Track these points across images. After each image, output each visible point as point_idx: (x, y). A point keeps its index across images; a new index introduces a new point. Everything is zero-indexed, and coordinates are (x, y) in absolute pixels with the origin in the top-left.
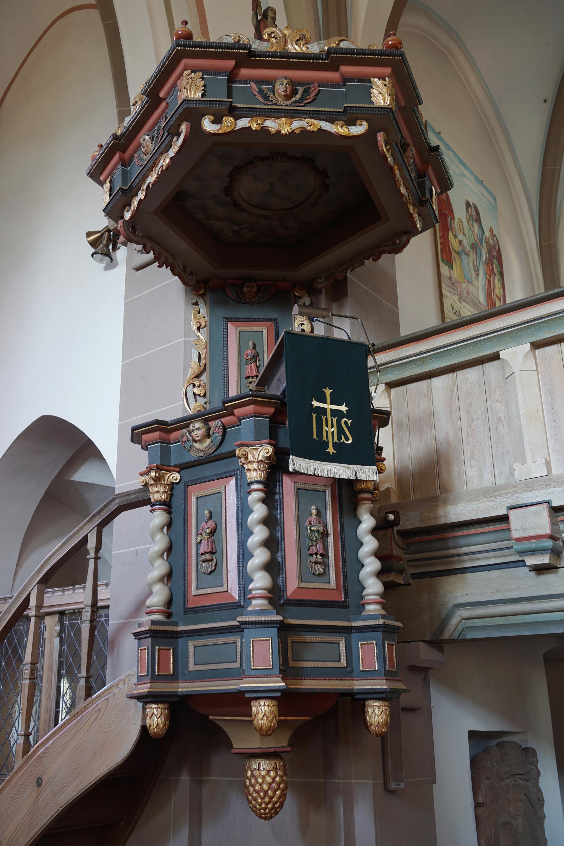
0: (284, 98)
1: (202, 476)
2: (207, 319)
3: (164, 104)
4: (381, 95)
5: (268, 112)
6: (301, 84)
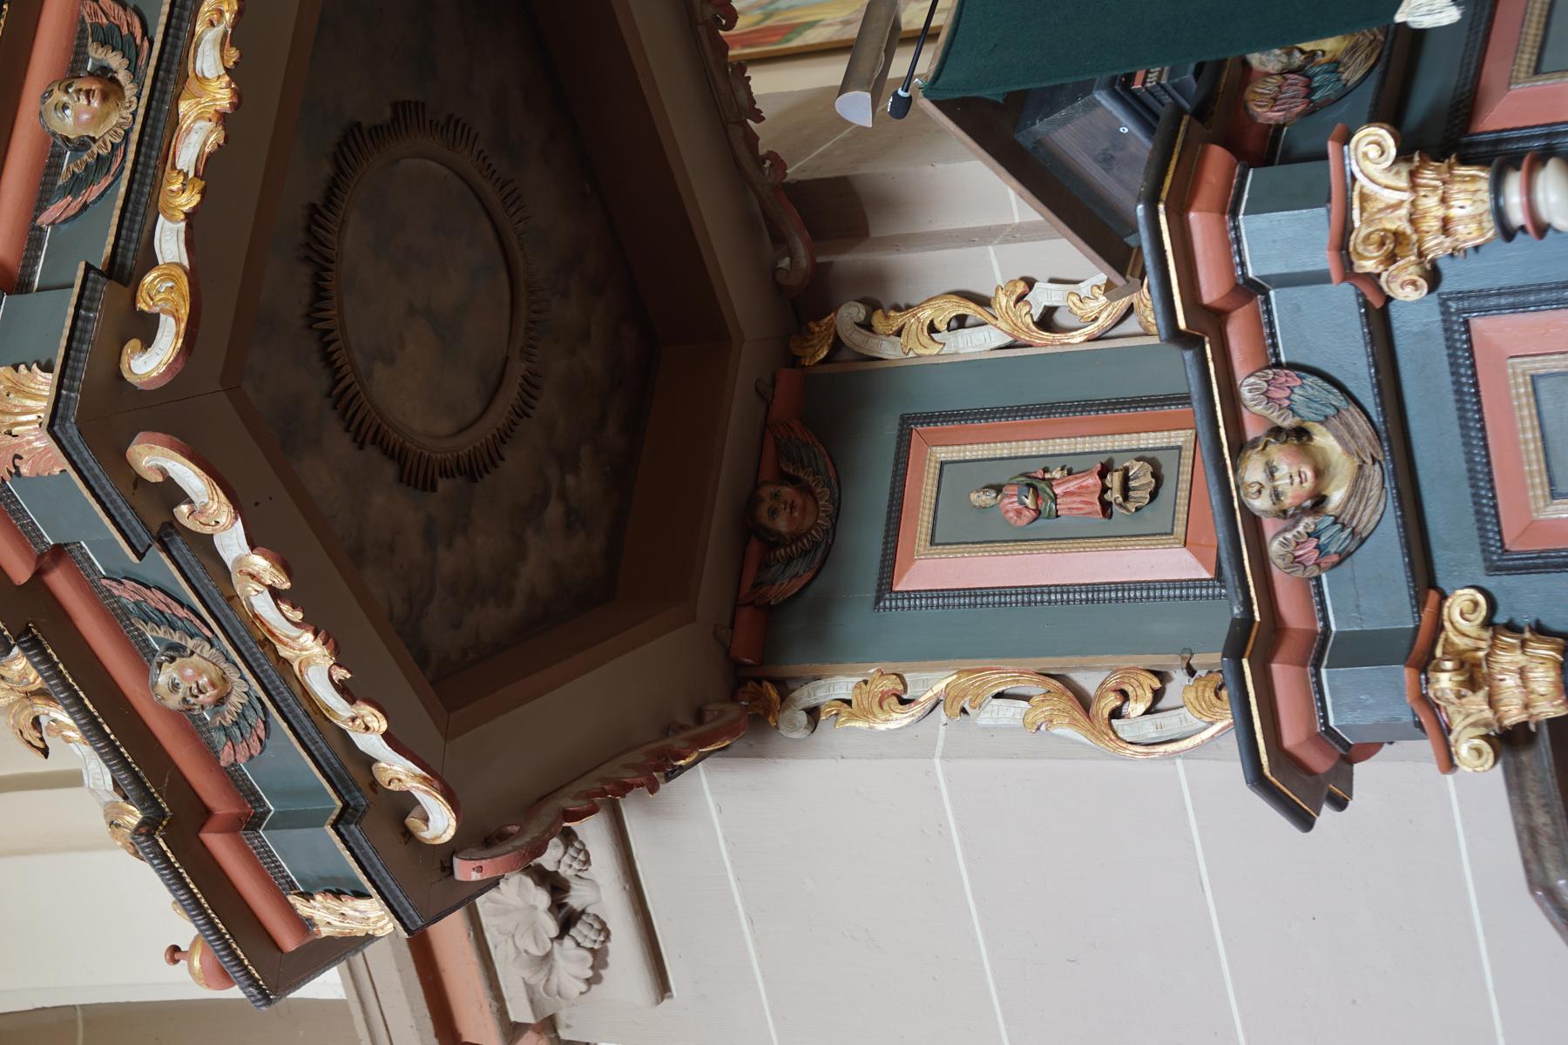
0: (111, 104)
1: (1465, 484)
3: (60, 582)
5: (148, 156)
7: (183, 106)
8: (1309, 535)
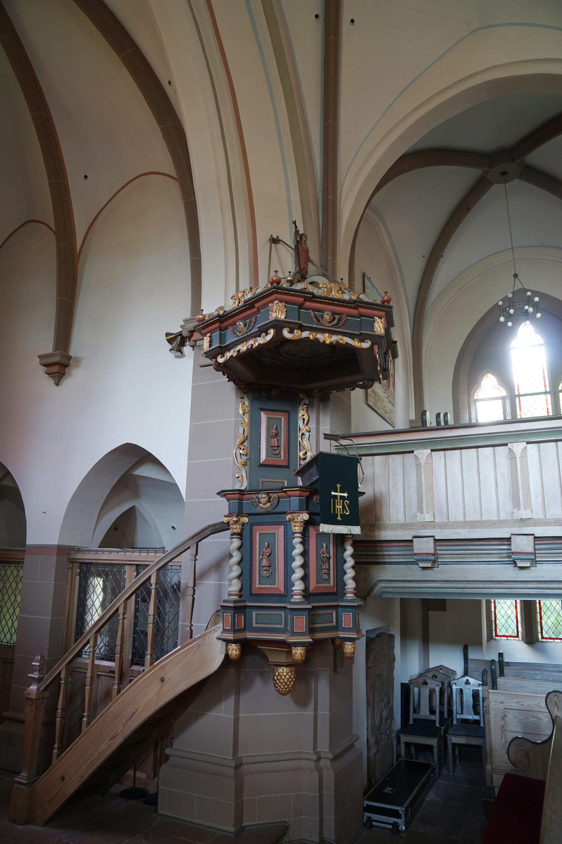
2: (249, 408)
4: (379, 327)
6: (337, 314)
7: (327, 334)
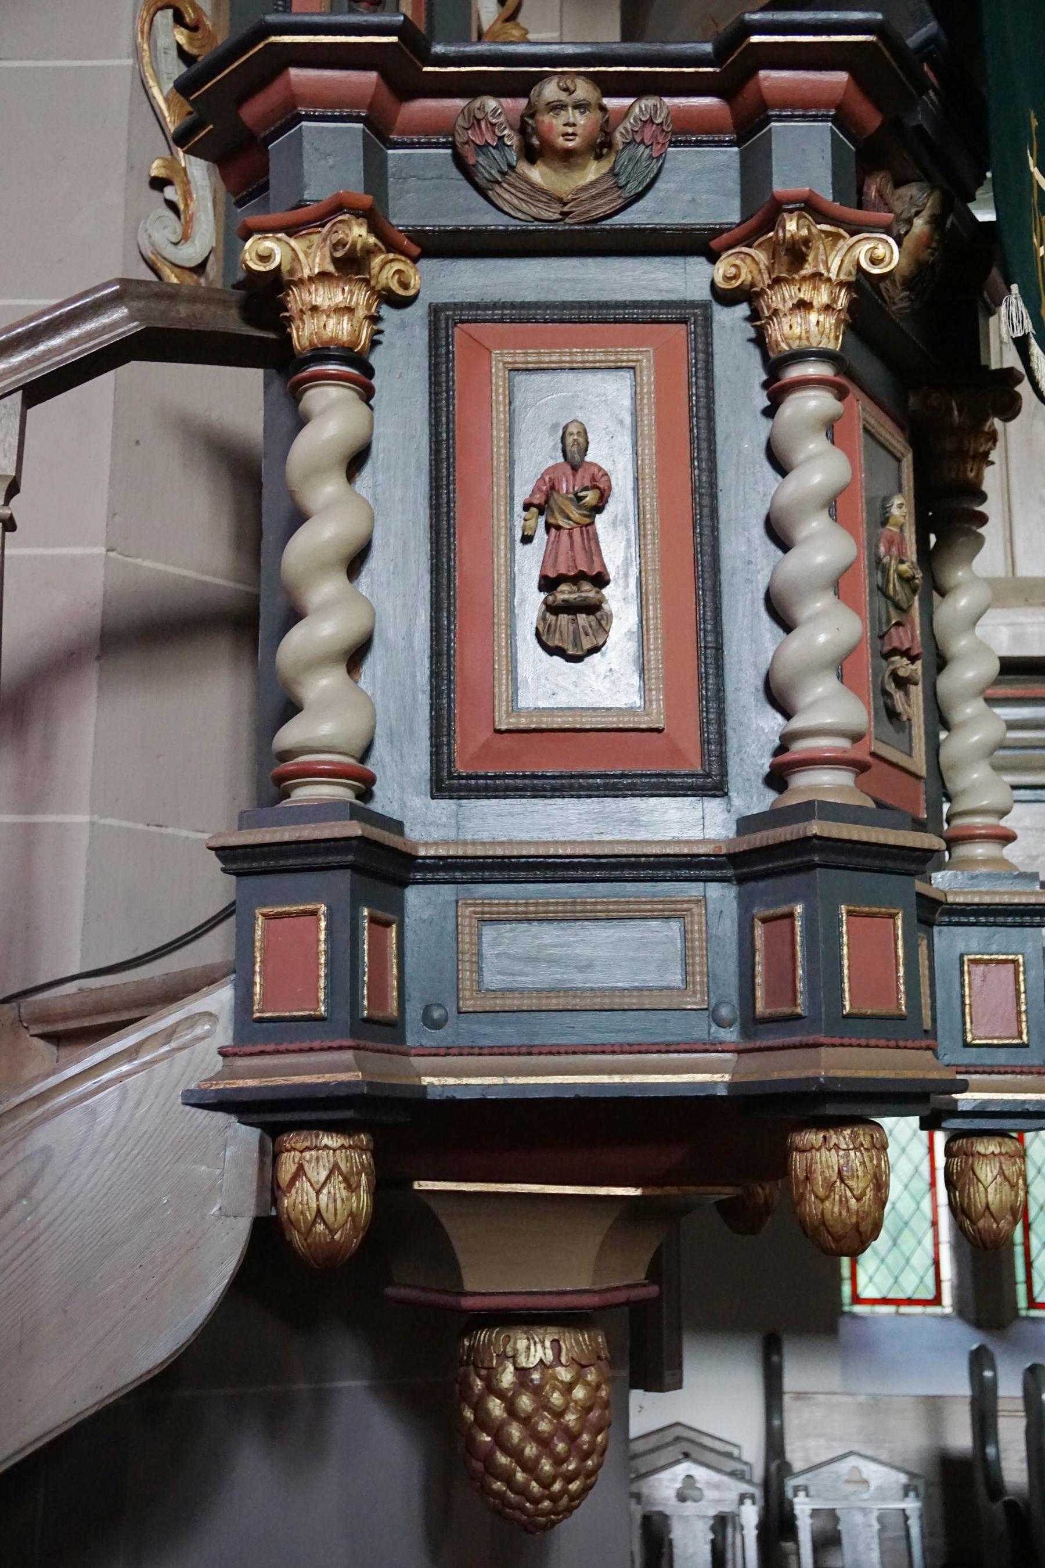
8: (501, 138)
